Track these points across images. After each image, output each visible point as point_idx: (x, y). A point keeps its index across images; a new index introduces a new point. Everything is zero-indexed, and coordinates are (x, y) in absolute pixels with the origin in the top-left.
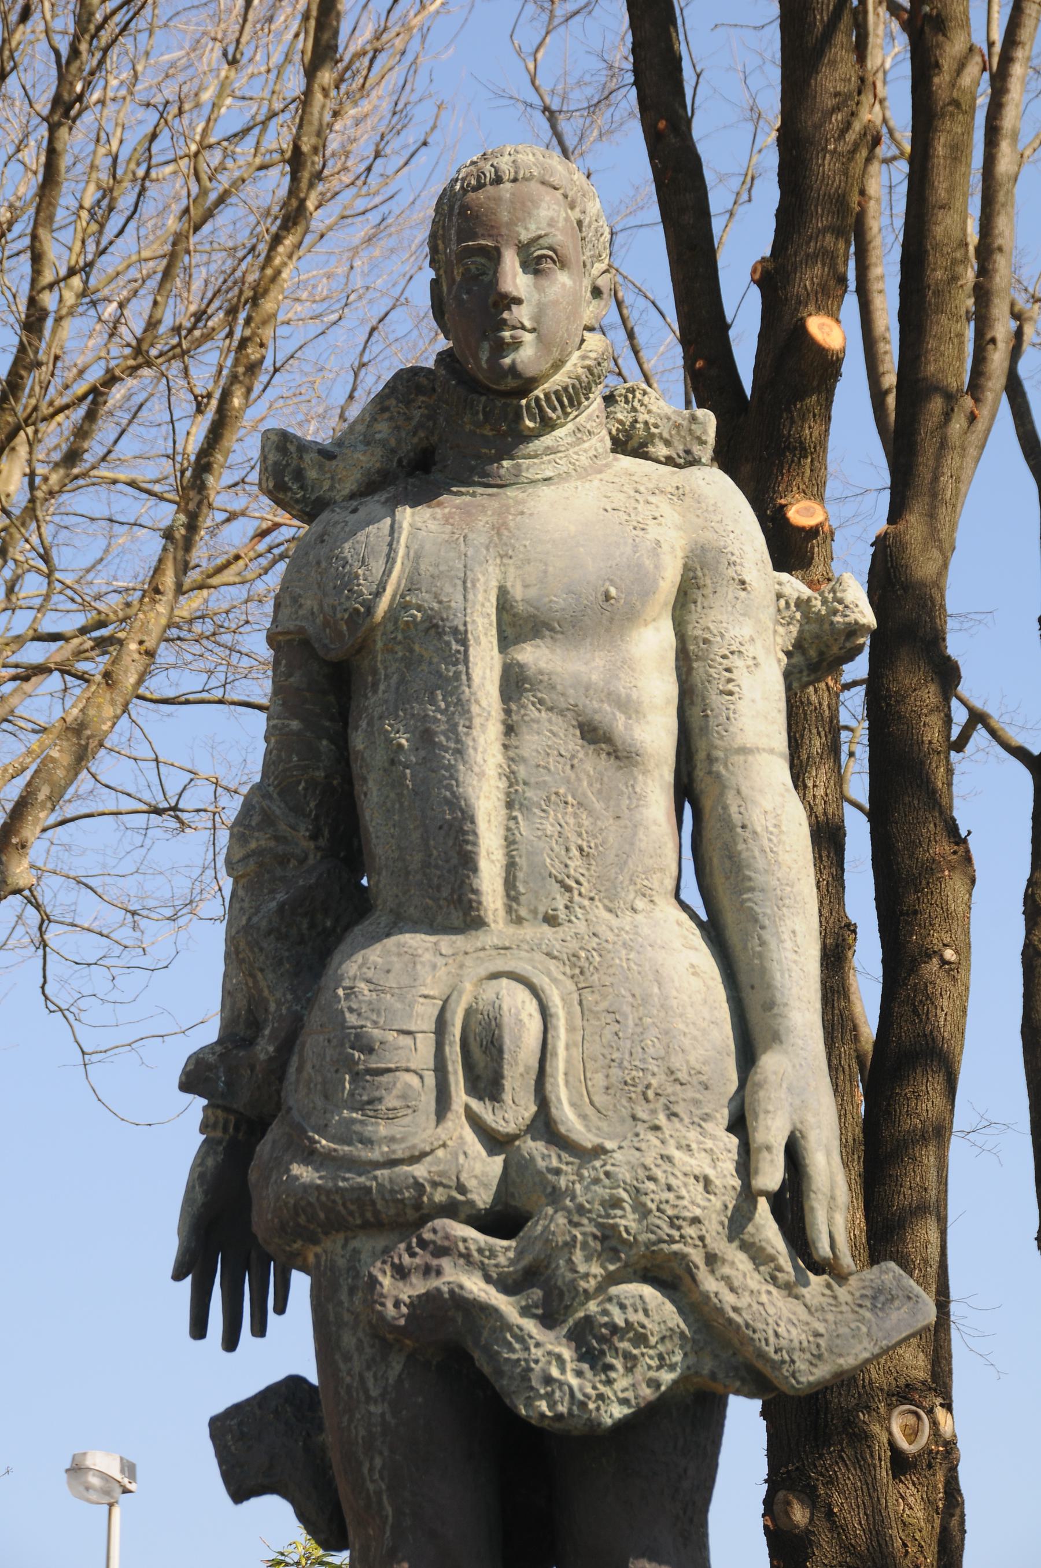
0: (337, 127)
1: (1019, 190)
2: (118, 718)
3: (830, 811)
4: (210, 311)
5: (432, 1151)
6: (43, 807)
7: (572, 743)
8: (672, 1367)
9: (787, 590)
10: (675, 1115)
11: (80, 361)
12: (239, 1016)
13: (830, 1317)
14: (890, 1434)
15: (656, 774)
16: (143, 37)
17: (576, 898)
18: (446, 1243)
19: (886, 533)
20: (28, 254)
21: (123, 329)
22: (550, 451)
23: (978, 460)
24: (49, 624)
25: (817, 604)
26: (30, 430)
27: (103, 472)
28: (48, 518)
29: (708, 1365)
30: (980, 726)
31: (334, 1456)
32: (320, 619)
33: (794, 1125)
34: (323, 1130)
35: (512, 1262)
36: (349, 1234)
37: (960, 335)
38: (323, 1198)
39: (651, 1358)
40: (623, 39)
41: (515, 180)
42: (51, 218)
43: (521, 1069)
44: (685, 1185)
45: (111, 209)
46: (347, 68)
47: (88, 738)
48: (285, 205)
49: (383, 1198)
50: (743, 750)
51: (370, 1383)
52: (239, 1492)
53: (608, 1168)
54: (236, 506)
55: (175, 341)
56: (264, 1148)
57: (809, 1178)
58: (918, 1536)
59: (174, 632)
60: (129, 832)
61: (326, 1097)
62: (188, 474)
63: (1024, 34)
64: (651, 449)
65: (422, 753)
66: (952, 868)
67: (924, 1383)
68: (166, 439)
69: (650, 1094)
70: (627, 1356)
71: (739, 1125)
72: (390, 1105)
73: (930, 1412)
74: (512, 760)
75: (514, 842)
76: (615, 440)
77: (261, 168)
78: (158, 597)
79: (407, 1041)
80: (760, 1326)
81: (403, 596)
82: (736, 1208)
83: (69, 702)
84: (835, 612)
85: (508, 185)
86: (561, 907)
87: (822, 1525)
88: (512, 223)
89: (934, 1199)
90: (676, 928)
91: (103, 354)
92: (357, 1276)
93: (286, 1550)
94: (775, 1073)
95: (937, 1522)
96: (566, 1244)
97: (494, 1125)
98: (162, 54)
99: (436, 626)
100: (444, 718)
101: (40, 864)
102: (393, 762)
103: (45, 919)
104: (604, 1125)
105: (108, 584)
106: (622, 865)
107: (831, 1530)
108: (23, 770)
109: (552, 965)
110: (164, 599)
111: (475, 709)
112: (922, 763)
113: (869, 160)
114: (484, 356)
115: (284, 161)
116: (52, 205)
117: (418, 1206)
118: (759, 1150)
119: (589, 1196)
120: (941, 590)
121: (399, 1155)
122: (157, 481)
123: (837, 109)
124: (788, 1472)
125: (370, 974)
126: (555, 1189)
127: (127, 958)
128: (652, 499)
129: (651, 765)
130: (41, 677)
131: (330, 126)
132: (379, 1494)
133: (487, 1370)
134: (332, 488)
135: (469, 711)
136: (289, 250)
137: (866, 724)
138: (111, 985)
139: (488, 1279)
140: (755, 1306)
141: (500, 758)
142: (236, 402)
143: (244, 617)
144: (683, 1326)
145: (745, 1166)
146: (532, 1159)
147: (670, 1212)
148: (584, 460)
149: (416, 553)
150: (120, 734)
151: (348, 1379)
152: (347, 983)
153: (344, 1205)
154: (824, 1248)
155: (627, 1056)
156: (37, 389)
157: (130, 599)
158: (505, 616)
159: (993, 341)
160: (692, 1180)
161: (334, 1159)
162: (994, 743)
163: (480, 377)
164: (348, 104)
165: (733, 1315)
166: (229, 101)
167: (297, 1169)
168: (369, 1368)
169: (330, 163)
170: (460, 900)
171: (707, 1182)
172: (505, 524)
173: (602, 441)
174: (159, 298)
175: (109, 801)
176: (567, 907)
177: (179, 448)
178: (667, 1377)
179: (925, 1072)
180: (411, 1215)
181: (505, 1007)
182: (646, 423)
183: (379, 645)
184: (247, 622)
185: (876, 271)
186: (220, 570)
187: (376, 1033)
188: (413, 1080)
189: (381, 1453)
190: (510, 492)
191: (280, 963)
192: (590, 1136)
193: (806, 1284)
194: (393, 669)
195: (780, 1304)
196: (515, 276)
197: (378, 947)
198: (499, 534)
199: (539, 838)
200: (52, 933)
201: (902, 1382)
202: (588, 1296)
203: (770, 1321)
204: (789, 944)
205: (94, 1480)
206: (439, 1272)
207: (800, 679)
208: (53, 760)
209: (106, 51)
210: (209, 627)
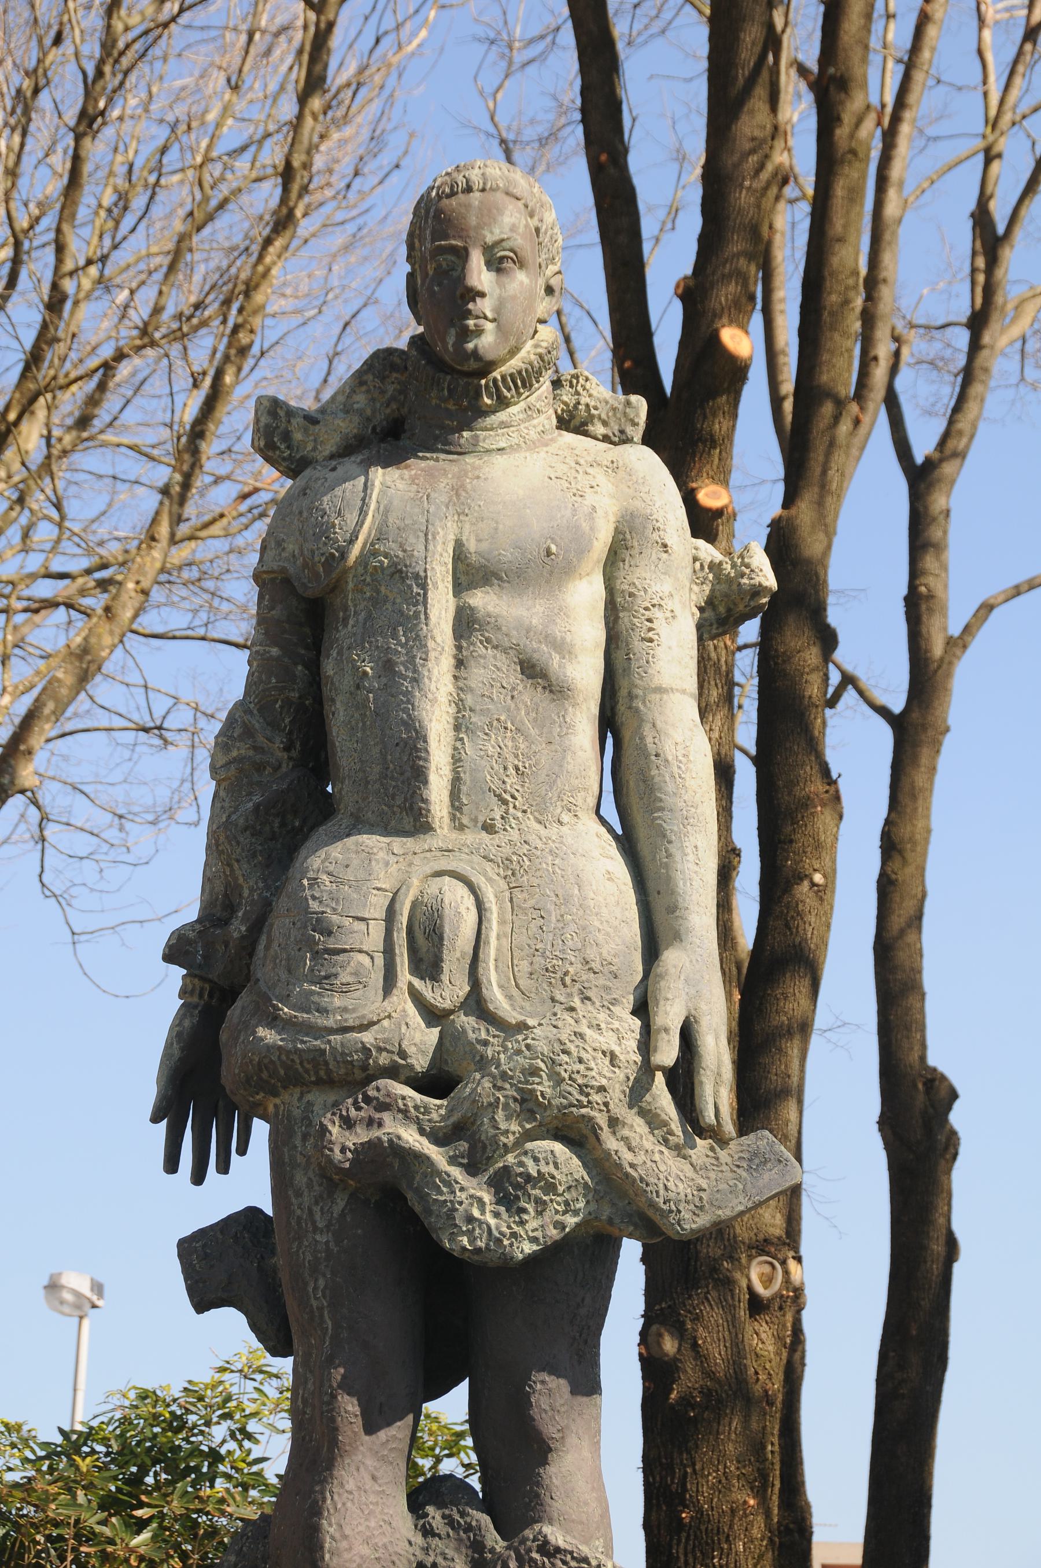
0: (323, 148)
1: (902, 231)
2: (115, 646)
3: (723, 752)
4: (207, 301)
5: (379, 1021)
6: (48, 720)
7: (513, 677)
8: (576, 1212)
9: (702, 555)
10: (588, 999)
11: (94, 341)
12: (217, 899)
13: (712, 1175)
14: (749, 1280)
15: (584, 707)
16: (158, 64)
17: (511, 810)
18: (388, 1100)
19: (780, 517)
20: (53, 246)
21: (131, 312)
22: (504, 425)
23: (858, 459)
24: (58, 565)
25: (727, 567)
26: (49, 396)
27: (109, 437)
28: (61, 474)
29: (606, 1212)
30: (850, 687)
31: (284, 1276)
32: (300, 561)
33: (689, 1011)
34: (285, 999)
35: (443, 1118)
36: (305, 1088)
37: (850, 351)
38: (284, 1057)
39: (559, 1204)
40: (571, 84)
41: (483, 190)
42: (73, 216)
43: (458, 955)
44: (594, 1058)
45: (126, 208)
46: (335, 96)
47: (89, 662)
48: (275, 213)
49: (335, 1059)
50: (660, 690)
51: (318, 1217)
52: (201, 1305)
53: (529, 1041)
54: (222, 471)
55: (175, 326)
56: (234, 1013)
57: (700, 1057)
58: (768, 1366)
59: (163, 577)
60: (119, 748)
61: (289, 971)
62: (184, 440)
63: (912, 98)
64: (591, 428)
65: (384, 680)
66: (824, 805)
67: (779, 1238)
68: (164, 411)
69: (568, 980)
70: (538, 1201)
71: (642, 1009)
72: (344, 981)
73: (783, 1263)
74: (461, 689)
75: (460, 760)
78: (154, 544)
79: (362, 926)
80: (652, 1180)
81: (372, 544)
82: (637, 1080)
83: (72, 633)
84: (743, 575)
85: (477, 194)
86: (498, 817)
87: (688, 1352)
88: (479, 227)
89: (795, 1084)
90: (596, 839)
91: (114, 334)
92: (310, 1124)
93: (232, 1359)
94: (675, 967)
95: (785, 1355)
96: (490, 1104)
97: (432, 1001)
98: (175, 80)
99: (400, 571)
100: (404, 651)
101: (41, 771)
102: (358, 687)
103: (44, 818)
104: (527, 1005)
105: (110, 533)
107: (695, 1359)
108: (32, 687)
109: (488, 866)
110: (159, 545)
111: (431, 644)
112: (803, 714)
113: (778, 198)
114: (451, 340)
115: (276, 175)
116: (75, 203)
117: (365, 1067)
118: (658, 1031)
119: (512, 1065)
120: (825, 568)
121: (350, 1023)
122: (153, 447)
123: (753, 151)
124: (662, 1309)
125: (331, 868)
127: (113, 855)
128: (590, 470)
130: (49, 610)
131: (317, 147)
132: (321, 1309)
133: (418, 1209)
134: (315, 449)
135: (426, 646)
136: (278, 251)
137: (756, 681)
138: (98, 876)
139: (422, 1132)
140: (649, 1163)
141: (451, 688)
142: (228, 379)
143: (225, 567)
144: (586, 1177)
145: (646, 1044)
146: (464, 1031)
147: (580, 1081)
148: (533, 435)
149: (385, 507)
151: (299, 1212)
152: (311, 875)
153: (301, 1063)
155: (549, 947)
156: (56, 361)
157: (128, 547)
158: (460, 565)
159: (876, 359)
160: (600, 1055)
161: (295, 1024)
162: (861, 701)
163: (447, 358)
164: (333, 128)
165: (629, 1170)
166: (230, 121)
167: (261, 1032)
168: (317, 1203)
169: (315, 180)
170: (411, 808)
171: (613, 1057)
172: (463, 486)
173: (549, 418)
174: (164, 288)
175: (103, 720)
176: (503, 818)
177: (176, 419)
178: (571, 1221)
179: (793, 977)
180: (359, 1075)
181: (446, 901)
182: (587, 405)
183: (351, 585)
184: (228, 571)
185: (779, 294)
186: (206, 526)
187: (335, 918)
188: (365, 960)
189: (324, 1275)
190: (469, 459)
191: (254, 856)
192: (514, 1014)
193: (693, 1147)
194: (362, 607)
195: (670, 1162)
196: (480, 273)
197: (340, 845)
198: (458, 495)
199: (482, 757)
200: (51, 831)
201: (761, 1237)
202: (507, 1149)
203: (661, 1176)
204: (691, 857)
205: (68, 1296)
206: (380, 1125)
207: (709, 632)
208: (58, 680)
209: (126, 73)
210: (195, 574)
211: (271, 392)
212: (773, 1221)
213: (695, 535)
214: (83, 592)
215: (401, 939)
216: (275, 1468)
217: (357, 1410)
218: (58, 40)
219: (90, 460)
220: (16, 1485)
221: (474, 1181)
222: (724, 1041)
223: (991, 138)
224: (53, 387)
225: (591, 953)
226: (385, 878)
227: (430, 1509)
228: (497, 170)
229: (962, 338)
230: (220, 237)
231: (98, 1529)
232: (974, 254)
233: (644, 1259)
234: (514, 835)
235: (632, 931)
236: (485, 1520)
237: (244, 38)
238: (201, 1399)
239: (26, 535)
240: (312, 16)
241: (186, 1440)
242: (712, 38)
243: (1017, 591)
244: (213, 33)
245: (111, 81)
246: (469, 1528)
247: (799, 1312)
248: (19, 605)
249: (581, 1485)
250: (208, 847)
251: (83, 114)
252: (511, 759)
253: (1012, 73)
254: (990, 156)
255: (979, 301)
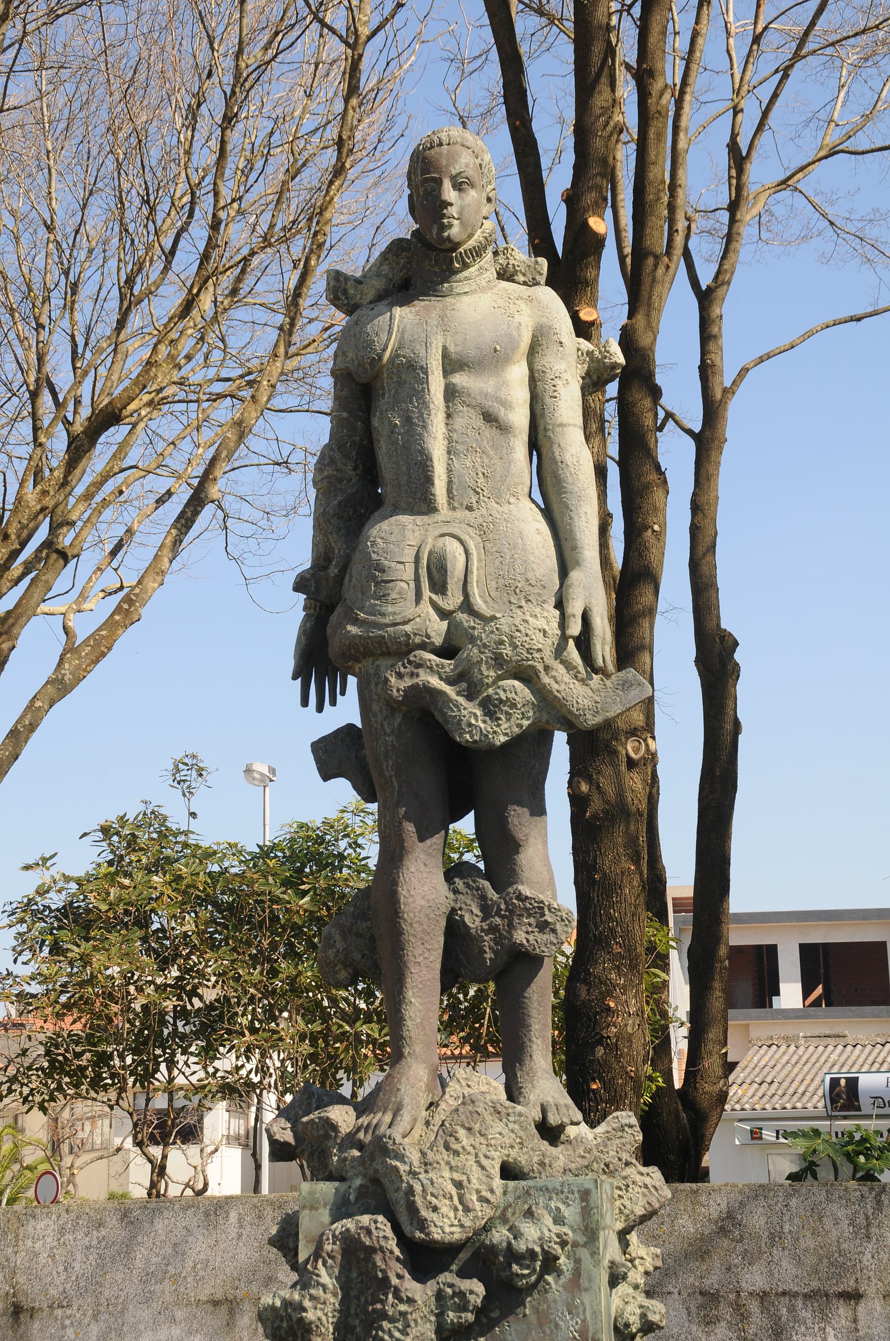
0: (360, 128)
7: (479, 422)
8: (528, 718)
9: (582, 347)
13: (603, 694)
22: (467, 279)
24: (224, 374)
25: (597, 353)
27: (248, 300)
29: (545, 717)
31: (370, 760)
34: (361, 609)
35: (452, 671)
37: (662, 227)
42: (223, 174)
45: (251, 169)
50: (561, 425)
51: (386, 727)
52: (326, 777)
54: (313, 316)
56: (334, 618)
63: (691, 80)
66: (658, 486)
70: (507, 713)
71: (560, 605)
73: (645, 740)
76: (498, 273)
77: (323, 148)
79: (401, 566)
80: (569, 699)
84: (605, 357)
87: (594, 791)
88: (448, 166)
92: (379, 677)
103: (226, 516)
104: (495, 606)
106: (504, 482)
109: (470, 529)
111: (432, 406)
113: (617, 141)
114: (435, 232)
117: (407, 644)
120: (653, 352)
121: (398, 621)
123: (602, 115)
125: (383, 535)
126: (472, 636)
129: (517, 433)
131: (357, 126)
132: (391, 777)
133: (441, 720)
139: (441, 679)
141: (444, 430)
148: (484, 283)
150: (259, 426)
152: (372, 539)
154: (600, 662)
159: (677, 231)
164: (365, 117)
167: (349, 628)
171: (545, 632)
175: (255, 460)
178: (526, 723)
180: (404, 649)
183: (385, 375)
185: (621, 197)
188: (405, 585)
190: (448, 299)
191: (340, 530)
193: (592, 679)
202: (488, 686)
204: (583, 519)
205: (257, 776)
206: (418, 676)
208: (228, 438)
209: (248, 92)
210: (301, 375)
211: (338, 268)
212: (638, 718)
213: (578, 336)
214: (239, 388)
215: (423, 572)
216: (372, 863)
217: (414, 829)
218: (210, 75)
219: (239, 313)
220: (237, 875)
221: (471, 704)
222: (606, 621)
223: (736, 101)
224: (215, 273)
225: (530, 575)
226: (413, 539)
227: (457, 880)
228: (456, 132)
229: (725, 216)
230: (305, 182)
231: (282, 896)
232: (730, 168)
233: (569, 742)
234: (484, 511)
235: (552, 562)
236: (487, 884)
237: (313, 66)
238: (332, 827)
239: (206, 358)
240: (349, 51)
241: (326, 848)
242: (576, 51)
243: (761, 360)
244: (296, 66)
245: (240, 96)
246: (478, 889)
247: (655, 766)
248: (205, 397)
249: (537, 863)
250: (314, 527)
251: (225, 116)
252: (480, 468)
253: (747, 63)
254: (736, 111)
255: (734, 195)
